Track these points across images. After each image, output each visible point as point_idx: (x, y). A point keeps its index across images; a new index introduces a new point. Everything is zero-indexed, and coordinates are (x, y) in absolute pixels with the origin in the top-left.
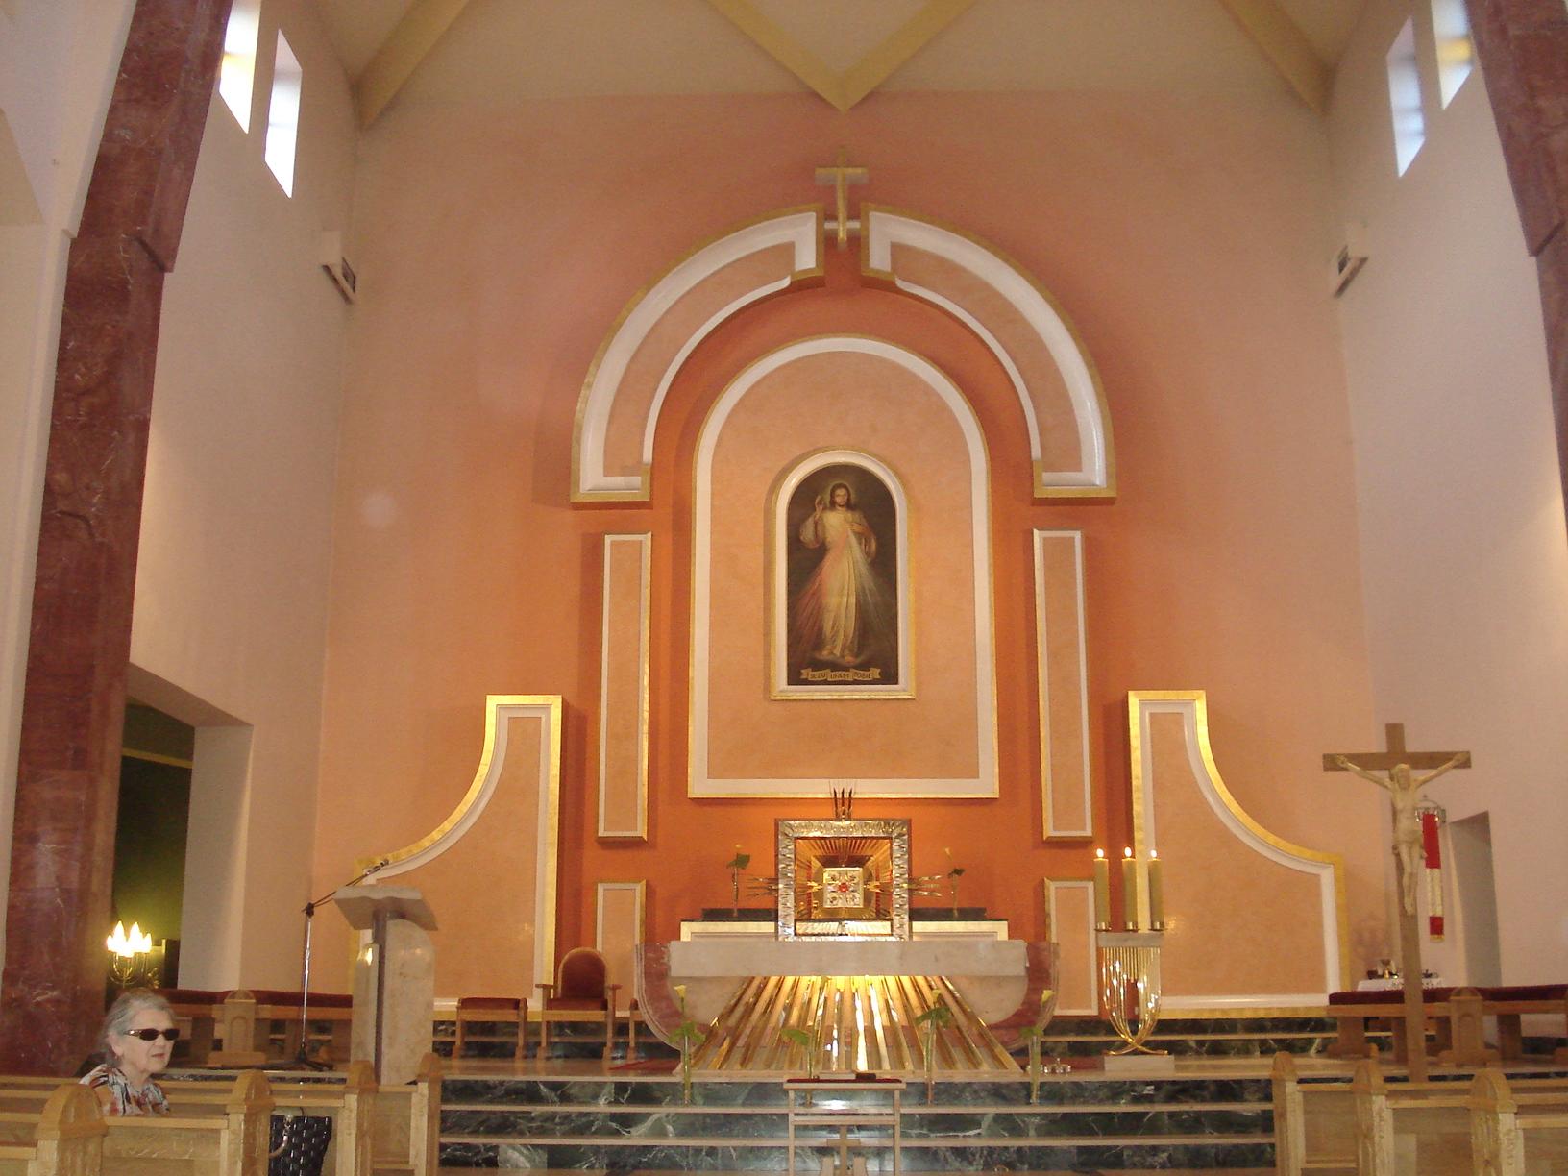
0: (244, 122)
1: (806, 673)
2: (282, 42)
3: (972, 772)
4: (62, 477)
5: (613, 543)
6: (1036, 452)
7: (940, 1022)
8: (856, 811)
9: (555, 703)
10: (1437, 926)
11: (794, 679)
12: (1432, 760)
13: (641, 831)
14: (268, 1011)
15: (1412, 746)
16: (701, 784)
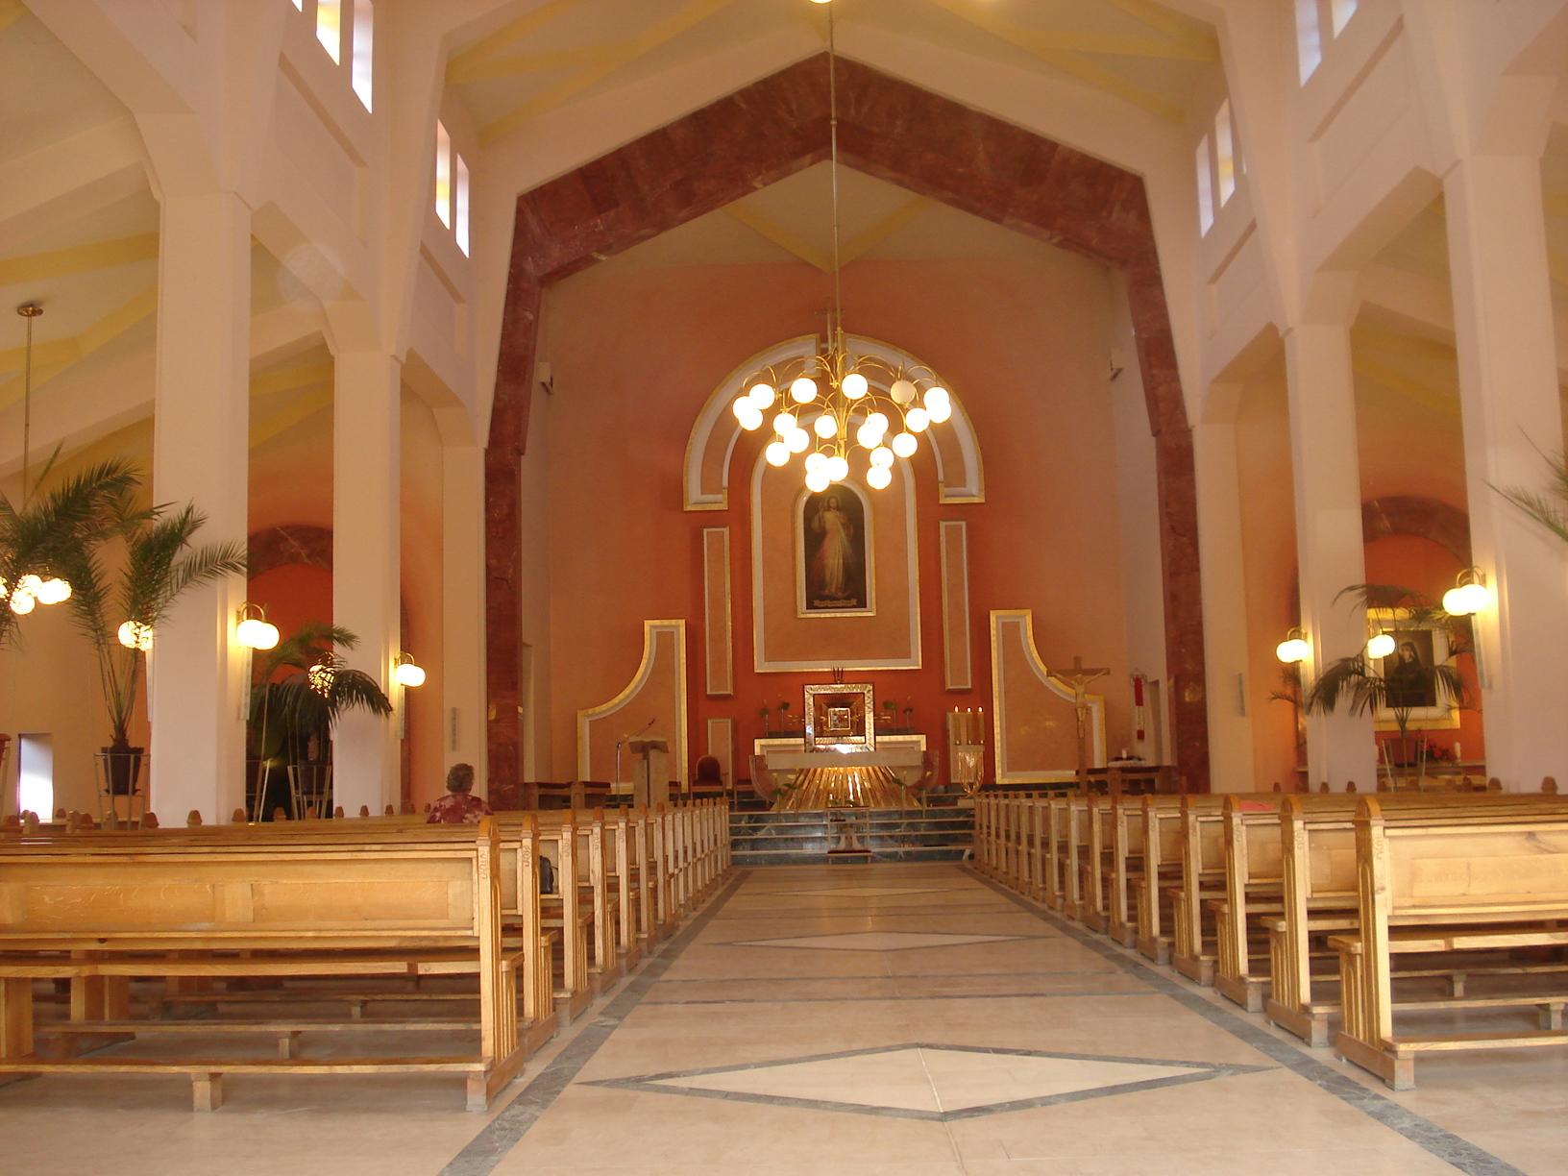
0: (447, 225)
1: (816, 603)
2: (459, 159)
3: (907, 655)
4: (493, 562)
5: (769, 658)
6: (941, 477)
7: (888, 786)
8: (845, 678)
9: (682, 622)
10: (1141, 735)
11: (810, 606)
12: (1093, 672)
13: (729, 691)
14: (590, 791)
15: (1084, 666)
16: (761, 666)
